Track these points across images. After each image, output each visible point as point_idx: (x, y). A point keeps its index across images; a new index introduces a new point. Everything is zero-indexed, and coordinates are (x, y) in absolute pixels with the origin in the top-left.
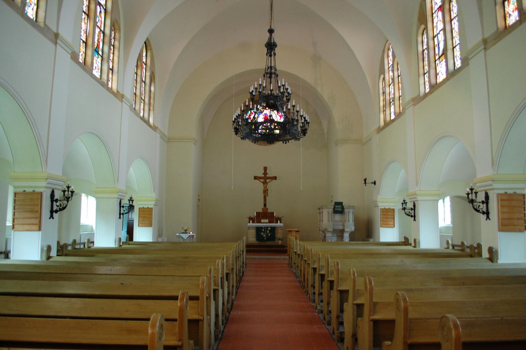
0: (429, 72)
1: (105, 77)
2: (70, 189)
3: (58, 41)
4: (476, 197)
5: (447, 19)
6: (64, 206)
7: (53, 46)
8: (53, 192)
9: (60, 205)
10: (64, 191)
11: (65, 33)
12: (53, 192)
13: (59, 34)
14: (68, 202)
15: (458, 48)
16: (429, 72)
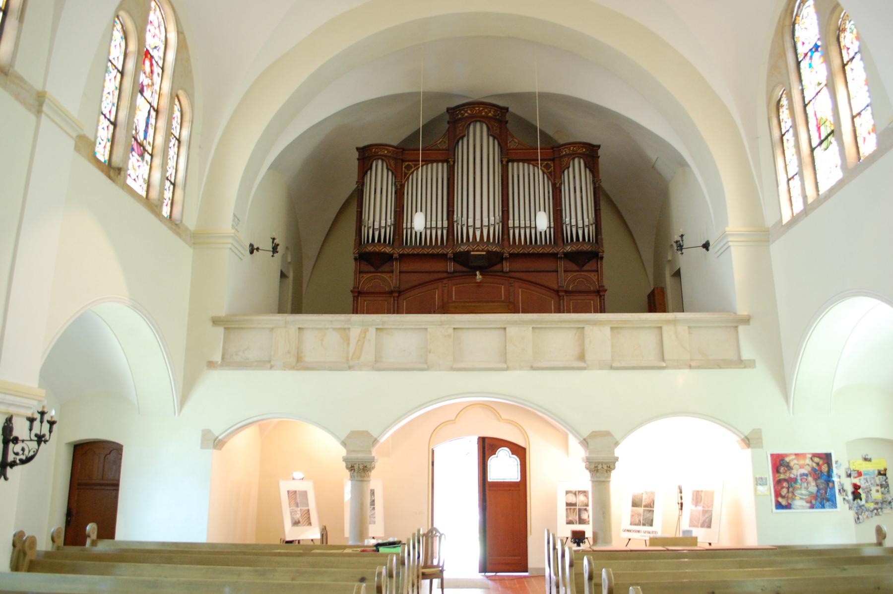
0: (800, 173)
1: (154, 194)
2: (47, 417)
3: (45, 108)
4: (50, 431)
5: (836, 63)
6: (32, 453)
7: (32, 118)
8: (9, 420)
9: (23, 449)
10: (32, 420)
11: (66, 93)
12: (9, 420)
13: (45, 92)
14: (39, 444)
15: (867, 116)
16: (800, 173)
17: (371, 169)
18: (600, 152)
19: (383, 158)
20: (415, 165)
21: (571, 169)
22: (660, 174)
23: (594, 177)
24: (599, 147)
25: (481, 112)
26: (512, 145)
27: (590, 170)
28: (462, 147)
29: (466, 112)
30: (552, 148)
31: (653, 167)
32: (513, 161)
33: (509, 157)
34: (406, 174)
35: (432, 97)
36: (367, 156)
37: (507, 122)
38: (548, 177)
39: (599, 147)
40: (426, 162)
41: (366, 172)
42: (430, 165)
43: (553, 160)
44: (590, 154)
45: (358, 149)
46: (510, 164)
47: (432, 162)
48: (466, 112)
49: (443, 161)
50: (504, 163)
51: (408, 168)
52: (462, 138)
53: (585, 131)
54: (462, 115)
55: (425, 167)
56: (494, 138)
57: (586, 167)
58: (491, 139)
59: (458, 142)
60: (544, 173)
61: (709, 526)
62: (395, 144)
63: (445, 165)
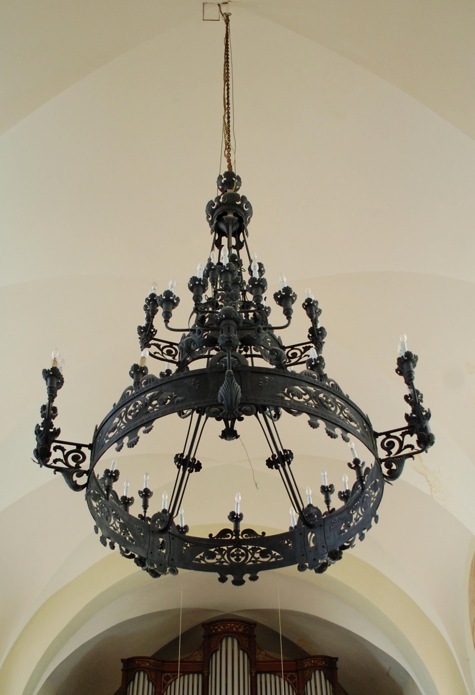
17: (134, 680)
18: (339, 664)
19: (145, 670)
20: (173, 676)
21: (218, 653)
22: (393, 681)
23: (334, 687)
24: (337, 659)
25: (232, 628)
26: (260, 657)
27: (330, 682)
28: (216, 659)
29: (219, 627)
30: (296, 661)
31: (387, 674)
32: (261, 673)
33: (256, 669)
34: (165, 684)
35: (189, 612)
36: (131, 667)
37: (255, 636)
38: (292, 688)
39: (337, 659)
40: (183, 673)
41: (129, 683)
42: (191, 676)
43: (297, 671)
44: (329, 665)
45: (123, 660)
46: (258, 676)
47: (188, 673)
48: (219, 627)
49: (198, 673)
50: (253, 674)
51: (167, 678)
52: (216, 652)
53: (326, 646)
54: (216, 630)
55: (182, 677)
56: (244, 652)
57: (239, 648)
58: (241, 652)
59: (212, 656)
60: (289, 684)
61: (204, 3)
62: (150, 655)
63: (200, 676)
